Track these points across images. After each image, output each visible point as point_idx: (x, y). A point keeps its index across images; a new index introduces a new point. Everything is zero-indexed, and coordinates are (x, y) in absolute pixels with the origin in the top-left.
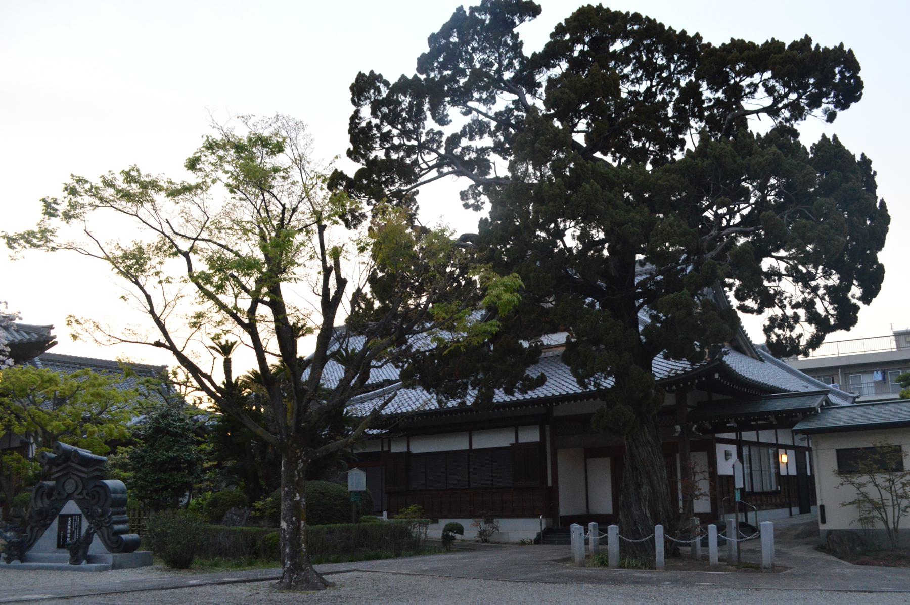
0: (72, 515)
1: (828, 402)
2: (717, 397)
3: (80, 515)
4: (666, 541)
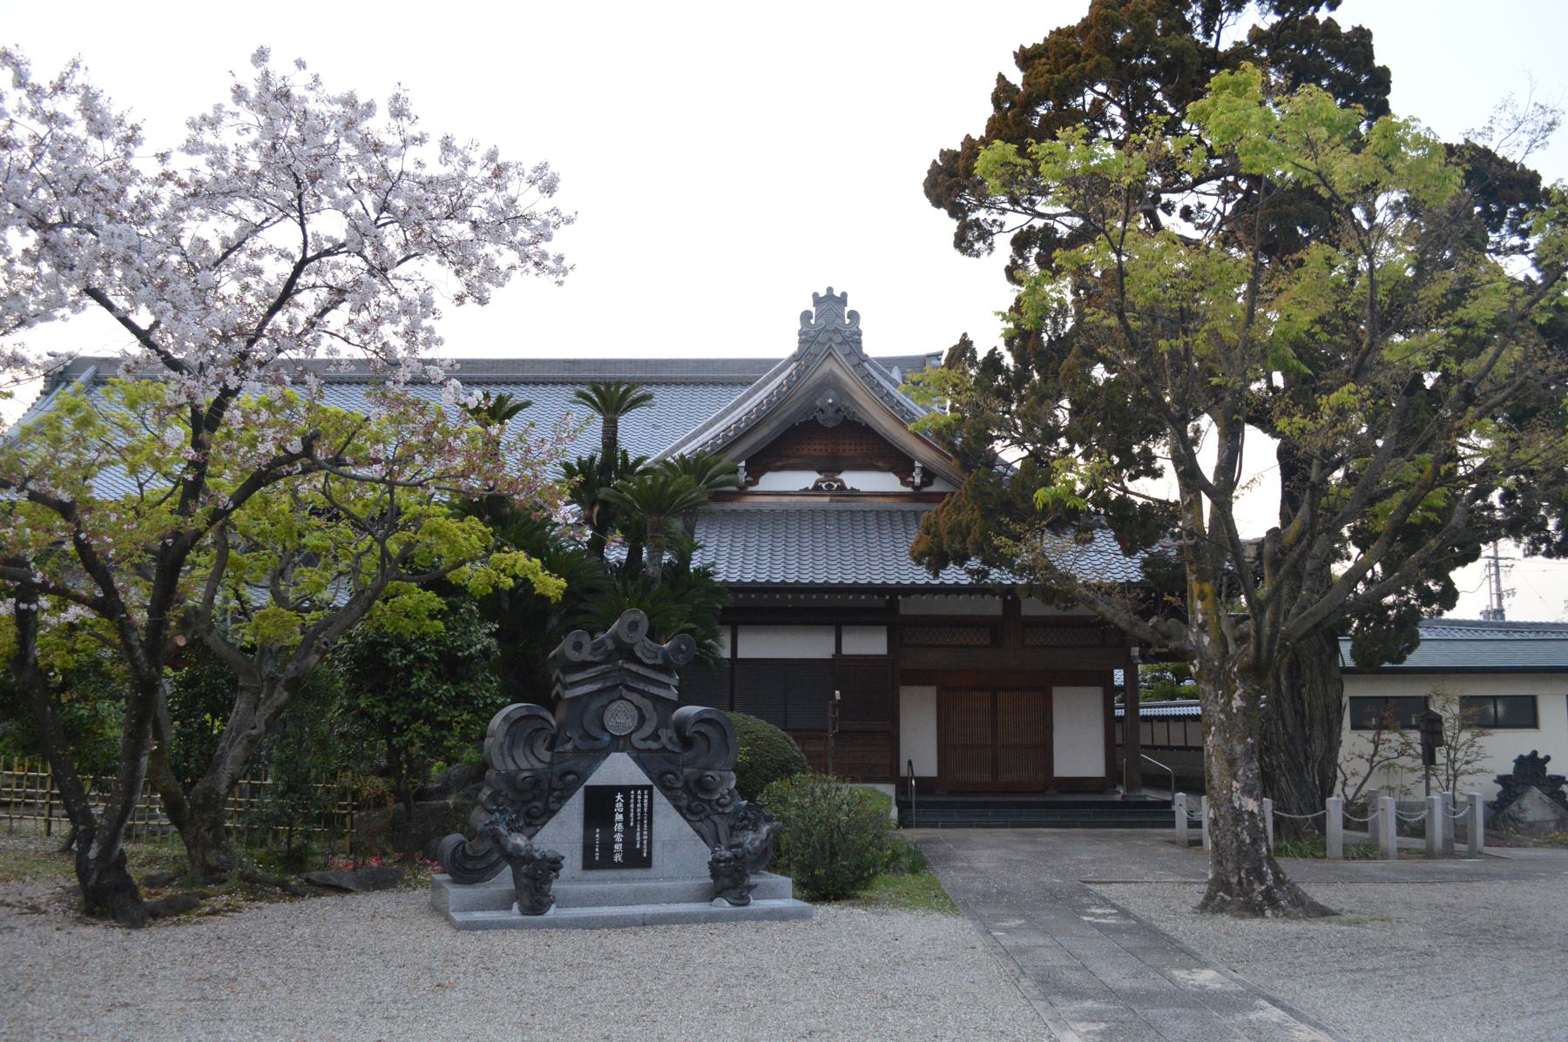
0: (626, 790)
3: (650, 788)
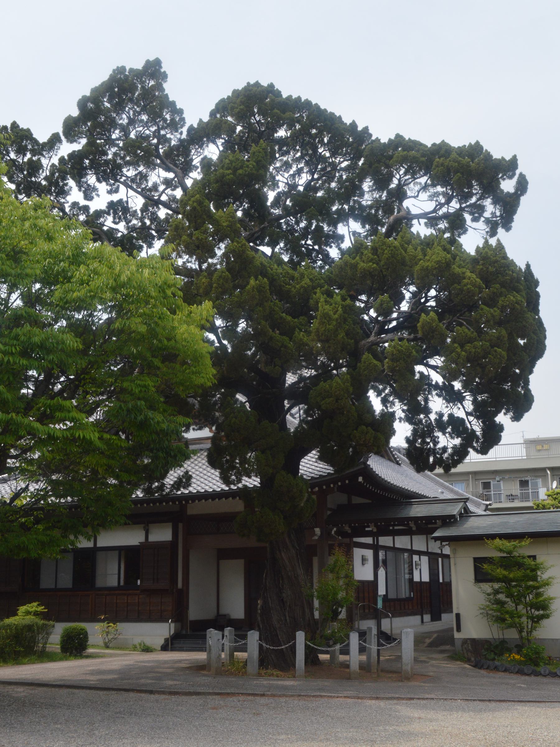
1: (466, 509)
2: (357, 500)
4: (307, 647)
